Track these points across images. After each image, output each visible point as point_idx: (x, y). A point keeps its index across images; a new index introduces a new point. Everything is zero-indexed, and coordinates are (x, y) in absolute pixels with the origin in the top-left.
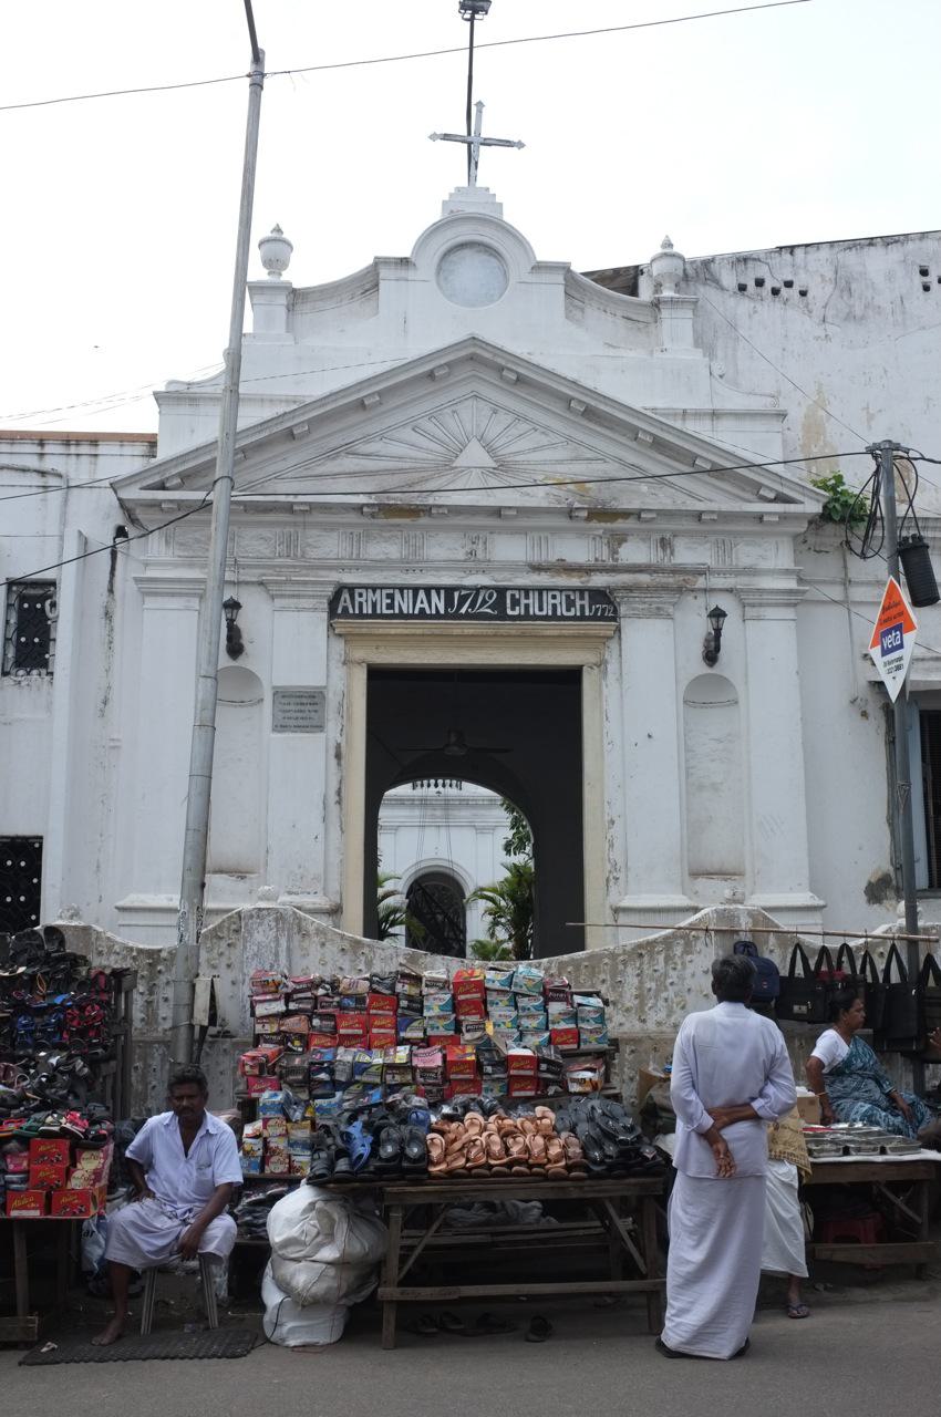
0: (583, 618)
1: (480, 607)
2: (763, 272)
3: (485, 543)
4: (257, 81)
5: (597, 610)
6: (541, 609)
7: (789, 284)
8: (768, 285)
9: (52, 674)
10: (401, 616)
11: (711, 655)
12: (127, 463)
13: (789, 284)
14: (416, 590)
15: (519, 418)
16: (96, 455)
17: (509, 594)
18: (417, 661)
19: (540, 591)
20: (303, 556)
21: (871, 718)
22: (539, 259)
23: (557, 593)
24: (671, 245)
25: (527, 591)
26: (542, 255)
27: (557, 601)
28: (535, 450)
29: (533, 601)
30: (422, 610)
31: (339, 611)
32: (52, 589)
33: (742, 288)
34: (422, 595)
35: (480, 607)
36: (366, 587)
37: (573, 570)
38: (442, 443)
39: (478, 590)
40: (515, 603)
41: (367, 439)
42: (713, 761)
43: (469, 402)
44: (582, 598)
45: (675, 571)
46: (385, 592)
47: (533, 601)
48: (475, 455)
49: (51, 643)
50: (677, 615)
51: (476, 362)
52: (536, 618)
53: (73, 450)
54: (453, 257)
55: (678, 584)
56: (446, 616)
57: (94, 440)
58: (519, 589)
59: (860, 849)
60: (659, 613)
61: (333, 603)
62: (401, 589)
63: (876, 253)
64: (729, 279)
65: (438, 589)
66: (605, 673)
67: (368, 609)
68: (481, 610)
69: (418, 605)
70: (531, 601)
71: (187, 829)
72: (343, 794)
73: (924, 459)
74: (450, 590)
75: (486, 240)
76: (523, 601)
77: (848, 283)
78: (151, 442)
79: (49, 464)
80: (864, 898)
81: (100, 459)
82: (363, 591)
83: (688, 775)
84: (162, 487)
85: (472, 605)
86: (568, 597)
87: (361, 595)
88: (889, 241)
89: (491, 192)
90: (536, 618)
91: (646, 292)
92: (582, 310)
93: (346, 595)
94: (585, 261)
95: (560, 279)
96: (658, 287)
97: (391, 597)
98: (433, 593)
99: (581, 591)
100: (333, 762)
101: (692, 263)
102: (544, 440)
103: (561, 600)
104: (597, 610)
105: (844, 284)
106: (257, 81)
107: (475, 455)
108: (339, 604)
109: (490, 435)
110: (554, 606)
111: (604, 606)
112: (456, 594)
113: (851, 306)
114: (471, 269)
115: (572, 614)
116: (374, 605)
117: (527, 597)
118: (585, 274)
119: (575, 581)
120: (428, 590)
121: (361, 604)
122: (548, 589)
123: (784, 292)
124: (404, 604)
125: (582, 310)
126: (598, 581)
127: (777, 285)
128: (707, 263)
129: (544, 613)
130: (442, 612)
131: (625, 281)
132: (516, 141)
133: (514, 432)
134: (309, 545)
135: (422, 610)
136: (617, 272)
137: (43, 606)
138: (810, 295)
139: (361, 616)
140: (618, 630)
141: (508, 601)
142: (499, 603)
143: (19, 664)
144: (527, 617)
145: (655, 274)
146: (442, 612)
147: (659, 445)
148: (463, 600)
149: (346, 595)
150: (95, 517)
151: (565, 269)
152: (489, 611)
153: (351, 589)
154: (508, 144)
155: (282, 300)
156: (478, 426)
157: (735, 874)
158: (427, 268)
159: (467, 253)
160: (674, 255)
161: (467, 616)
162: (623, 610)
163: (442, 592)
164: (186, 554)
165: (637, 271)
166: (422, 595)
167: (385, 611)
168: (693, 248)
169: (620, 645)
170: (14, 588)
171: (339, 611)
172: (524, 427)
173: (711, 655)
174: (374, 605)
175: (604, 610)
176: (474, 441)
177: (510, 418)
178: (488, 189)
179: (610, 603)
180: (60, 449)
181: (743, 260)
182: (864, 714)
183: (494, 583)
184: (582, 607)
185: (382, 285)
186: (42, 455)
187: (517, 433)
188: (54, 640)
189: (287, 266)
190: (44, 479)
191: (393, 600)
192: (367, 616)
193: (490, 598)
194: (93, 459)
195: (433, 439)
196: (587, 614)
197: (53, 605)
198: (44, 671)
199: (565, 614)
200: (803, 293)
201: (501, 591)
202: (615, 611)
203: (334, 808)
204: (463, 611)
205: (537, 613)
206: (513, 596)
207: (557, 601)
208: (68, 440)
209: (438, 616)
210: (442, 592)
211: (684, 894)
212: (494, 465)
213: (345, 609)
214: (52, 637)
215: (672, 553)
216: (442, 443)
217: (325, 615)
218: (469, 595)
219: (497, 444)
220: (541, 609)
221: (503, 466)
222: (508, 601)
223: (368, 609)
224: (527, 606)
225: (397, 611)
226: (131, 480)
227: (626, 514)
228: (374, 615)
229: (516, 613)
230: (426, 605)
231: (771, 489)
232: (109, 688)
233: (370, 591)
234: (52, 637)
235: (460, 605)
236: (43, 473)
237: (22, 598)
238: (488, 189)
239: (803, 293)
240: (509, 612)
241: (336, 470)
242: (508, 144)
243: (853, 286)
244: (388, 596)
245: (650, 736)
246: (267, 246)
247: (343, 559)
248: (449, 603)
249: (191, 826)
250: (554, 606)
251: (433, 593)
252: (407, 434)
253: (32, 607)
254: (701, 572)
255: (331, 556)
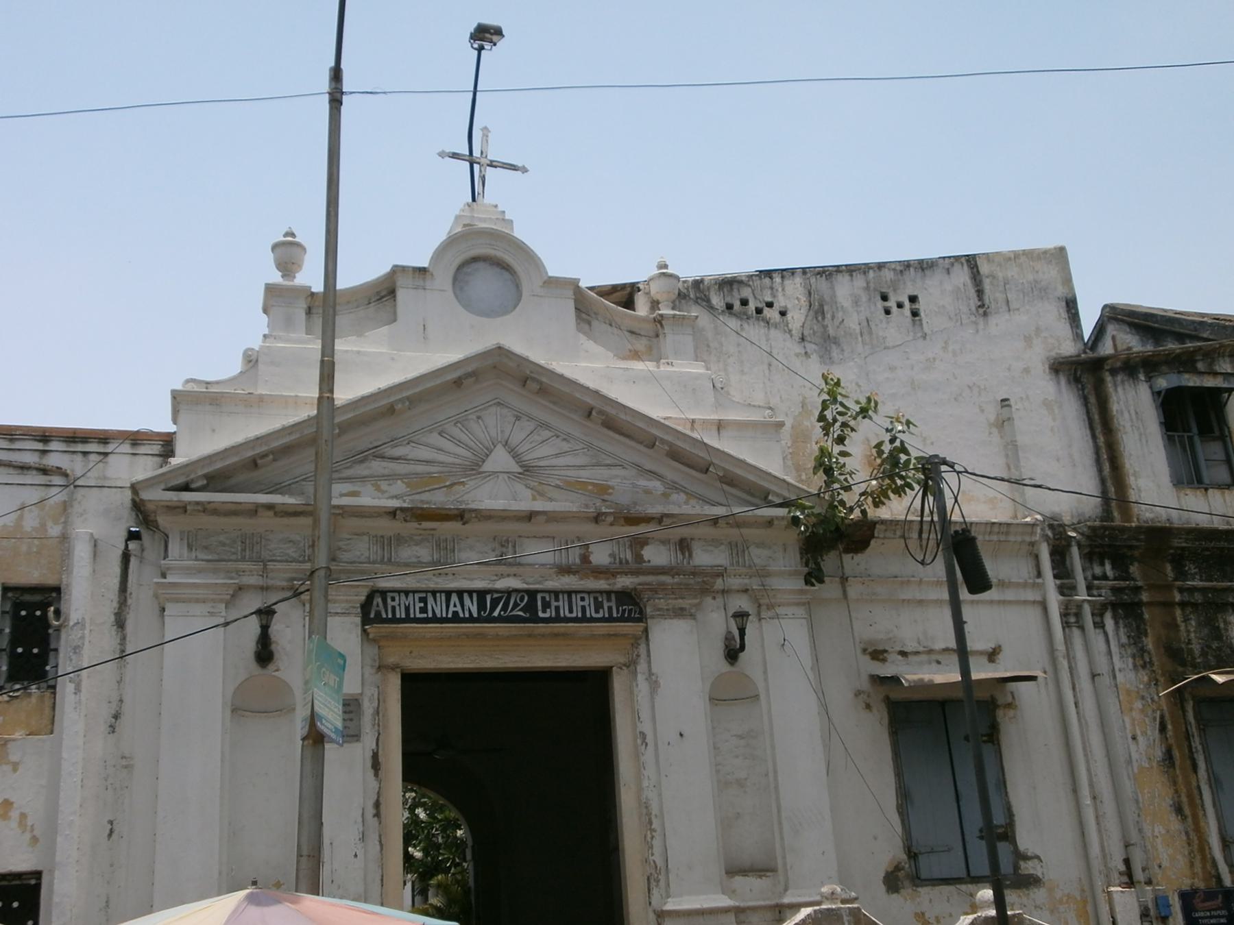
0: (610, 619)
1: (513, 609)
2: (746, 293)
3: (514, 547)
4: (336, 101)
5: (624, 611)
6: (571, 611)
7: (770, 305)
8: (752, 306)
9: (54, 687)
10: (435, 619)
11: (733, 653)
12: (143, 468)
13: (770, 305)
14: (448, 594)
15: (544, 425)
16: (106, 454)
17: (539, 597)
18: (452, 666)
19: (570, 593)
20: (390, 560)
21: (875, 710)
22: (550, 274)
23: (586, 596)
24: (666, 266)
25: (556, 594)
26: (554, 270)
27: (586, 603)
28: (557, 455)
29: (563, 603)
30: (455, 613)
31: (372, 616)
32: (54, 595)
33: (729, 307)
34: (454, 598)
35: (513, 609)
36: (399, 592)
37: (601, 573)
38: (468, 448)
39: (509, 593)
40: (546, 605)
41: (394, 441)
42: (737, 757)
43: (493, 409)
44: (609, 600)
45: (694, 573)
46: (417, 596)
47: (563, 603)
48: (500, 460)
49: (52, 654)
50: (699, 616)
51: (501, 372)
52: (592, 620)
53: (80, 447)
54: (467, 270)
55: (705, 584)
56: (478, 620)
57: (104, 438)
58: (549, 592)
59: (875, 838)
60: (680, 613)
61: (366, 606)
62: (434, 593)
63: (843, 279)
64: (717, 301)
65: (470, 593)
66: (635, 673)
67: (401, 614)
68: (514, 613)
69: (452, 609)
70: (561, 603)
71: (300, 855)
72: (382, 807)
73: (966, 472)
74: (482, 594)
75: (499, 254)
76: (554, 604)
77: (821, 306)
78: (167, 445)
79: (53, 460)
80: (883, 888)
81: (111, 458)
82: (396, 595)
83: (718, 771)
84: (186, 488)
85: (505, 608)
86: (596, 599)
87: (393, 599)
88: (851, 270)
89: (500, 208)
90: (592, 620)
91: (642, 308)
92: (589, 323)
93: (378, 600)
94: (594, 276)
95: (570, 293)
96: (655, 304)
97: (424, 600)
98: (466, 596)
99: (608, 593)
100: (371, 773)
101: (684, 282)
102: (565, 446)
103: (589, 602)
104: (624, 611)
105: (818, 309)
106: (336, 101)
107: (500, 460)
108: (373, 612)
109: (514, 441)
110: (583, 608)
111: (631, 607)
112: (488, 598)
113: (825, 327)
114: (485, 283)
115: (600, 615)
116: (407, 609)
117: (557, 600)
118: (591, 289)
119: (602, 584)
120: (460, 593)
121: (394, 608)
122: (576, 592)
123: (766, 311)
124: (437, 607)
125: (589, 323)
126: (624, 582)
127: (760, 305)
128: (698, 284)
129: (574, 615)
130: (475, 615)
131: (625, 295)
132: (520, 165)
133: (536, 437)
134: (340, 549)
135: (455, 613)
136: (615, 289)
137: (45, 614)
138: (789, 316)
139: (394, 620)
140: (646, 631)
141: (539, 603)
142: (529, 607)
143: (12, 677)
144: (558, 619)
145: (653, 293)
146: (475, 615)
147: (675, 455)
148: (495, 603)
149: (378, 600)
150: (98, 522)
151: (574, 284)
152: (521, 613)
153: (383, 593)
154: (513, 168)
155: (302, 305)
156: (502, 432)
157: (767, 871)
158: (443, 279)
159: (480, 265)
160: (671, 276)
161: (500, 619)
162: (649, 610)
163: (475, 595)
164: (210, 557)
165: (633, 288)
166: (454, 598)
167: (418, 615)
168: (688, 269)
169: (648, 645)
170: (10, 595)
171: (372, 616)
172: (547, 434)
173: (733, 653)
174: (407, 609)
175: (630, 611)
176: (499, 446)
177: (530, 426)
178: (496, 206)
179: (636, 604)
180: (126, 448)
181: (727, 284)
182: (868, 706)
183: (525, 586)
184: (610, 608)
185: (401, 294)
186: (44, 452)
187: (540, 439)
188: (56, 650)
189: (300, 267)
190: (48, 478)
191: (426, 604)
192: (401, 621)
193: (522, 599)
194: (102, 457)
195: (459, 443)
196: (615, 615)
197: (58, 613)
198: (44, 685)
199: (594, 615)
200: (783, 314)
201: (532, 594)
202: (641, 612)
203: (372, 822)
204: (496, 614)
205: (568, 615)
206: (543, 599)
207: (586, 603)
208: (74, 437)
209: (471, 619)
210: (475, 595)
211: (723, 893)
212: (520, 470)
213: (378, 613)
214: (52, 646)
215: (690, 556)
216: (468, 448)
217: (358, 620)
218: (500, 598)
219: (521, 450)
220: (571, 611)
221: (527, 471)
222: (539, 603)
223: (401, 614)
224: (557, 608)
225: (430, 615)
226: (150, 483)
227: (648, 519)
228: (408, 619)
229: (547, 615)
230: (459, 609)
231: (778, 495)
232: (121, 701)
233: (403, 595)
234: (52, 646)
235: (493, 609)
236: (44, 471)
237: (18, 606)
238: (496, 206)
239: (783, 314)
240: (541, 614)
241: (366, 473)
242: (513, 168)
243: (826, 308)
244: (421, 600)
245: (681, 735)
246: (278, 250)
247: (374, 562)
248: (481, 606)
249: (305, 853)
250: (583, 608)
251: (466, 596)
252: (435, 439)
253: (31, 614)
254: (720, 573)
255: (363, 559)
